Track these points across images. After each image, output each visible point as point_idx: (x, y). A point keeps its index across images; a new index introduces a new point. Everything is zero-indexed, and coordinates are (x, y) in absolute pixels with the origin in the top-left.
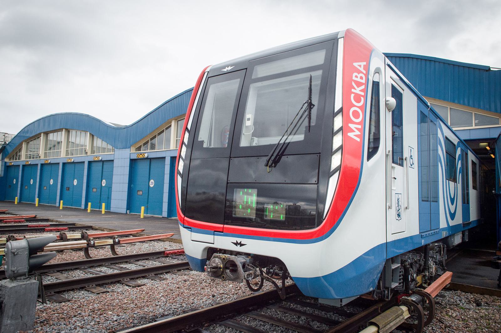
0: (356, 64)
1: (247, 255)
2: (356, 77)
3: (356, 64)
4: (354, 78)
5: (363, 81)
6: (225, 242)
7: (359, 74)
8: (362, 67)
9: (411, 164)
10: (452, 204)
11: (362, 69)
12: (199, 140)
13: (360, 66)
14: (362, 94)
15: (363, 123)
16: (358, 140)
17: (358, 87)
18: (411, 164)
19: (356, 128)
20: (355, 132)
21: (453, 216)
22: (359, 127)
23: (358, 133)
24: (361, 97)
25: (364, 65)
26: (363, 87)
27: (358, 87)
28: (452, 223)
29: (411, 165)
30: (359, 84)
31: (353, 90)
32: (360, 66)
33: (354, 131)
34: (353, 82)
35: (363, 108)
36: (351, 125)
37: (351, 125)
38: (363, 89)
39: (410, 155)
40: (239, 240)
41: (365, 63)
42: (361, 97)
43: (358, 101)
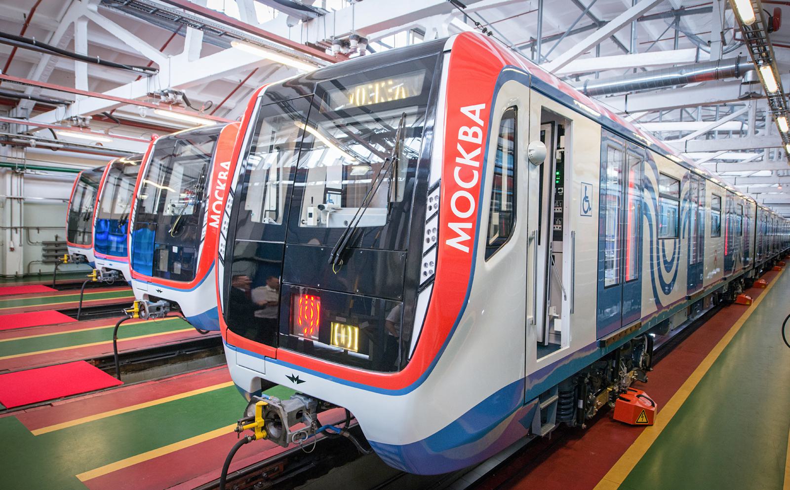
0: (465, 110)
1: (307, 397)
2: (466, 133)
3: (465, 110)
4: (461, 137)
5: (479, 141)
6: (278, 373)
7: (470, 128)
8: (478, 113)
9: (586, 210)
10: (668, 270)
11: (476, 118)
12: (247, 208)
13: (473, 112)
14: (476, 164)
15: (475, 219)
16: (466, 249)
17: (468, 151)
18: (586, 210)
19: (462, 229)
20: (461, 236)
21: (667, 288)
22: (469, 226)
23: (465, 237)
24: (474, 171)
25: (481, 110)
26: (478, 152)
27: (468, 151)
28: (665, 300)
29: (586, 212)
30: (470, 147)
31: (458, 160)
32: (473, 112)
33: (458, 235)
34: (458, 144)
35: (477, 192)
36: (453, 226)
37: (453, 226)
38: (478, 156)
39: (583, 196)
40: (296, 373)
41: (483, 106)
42: (474, 171)
43: (467, 177)
